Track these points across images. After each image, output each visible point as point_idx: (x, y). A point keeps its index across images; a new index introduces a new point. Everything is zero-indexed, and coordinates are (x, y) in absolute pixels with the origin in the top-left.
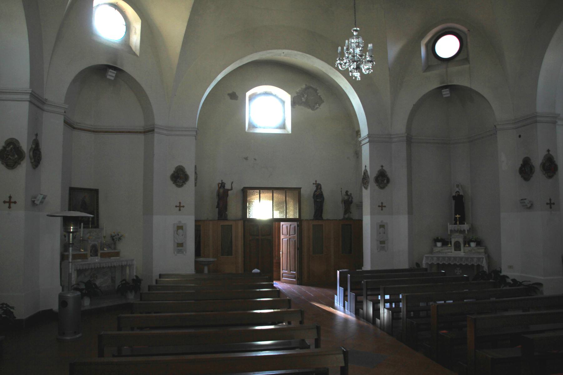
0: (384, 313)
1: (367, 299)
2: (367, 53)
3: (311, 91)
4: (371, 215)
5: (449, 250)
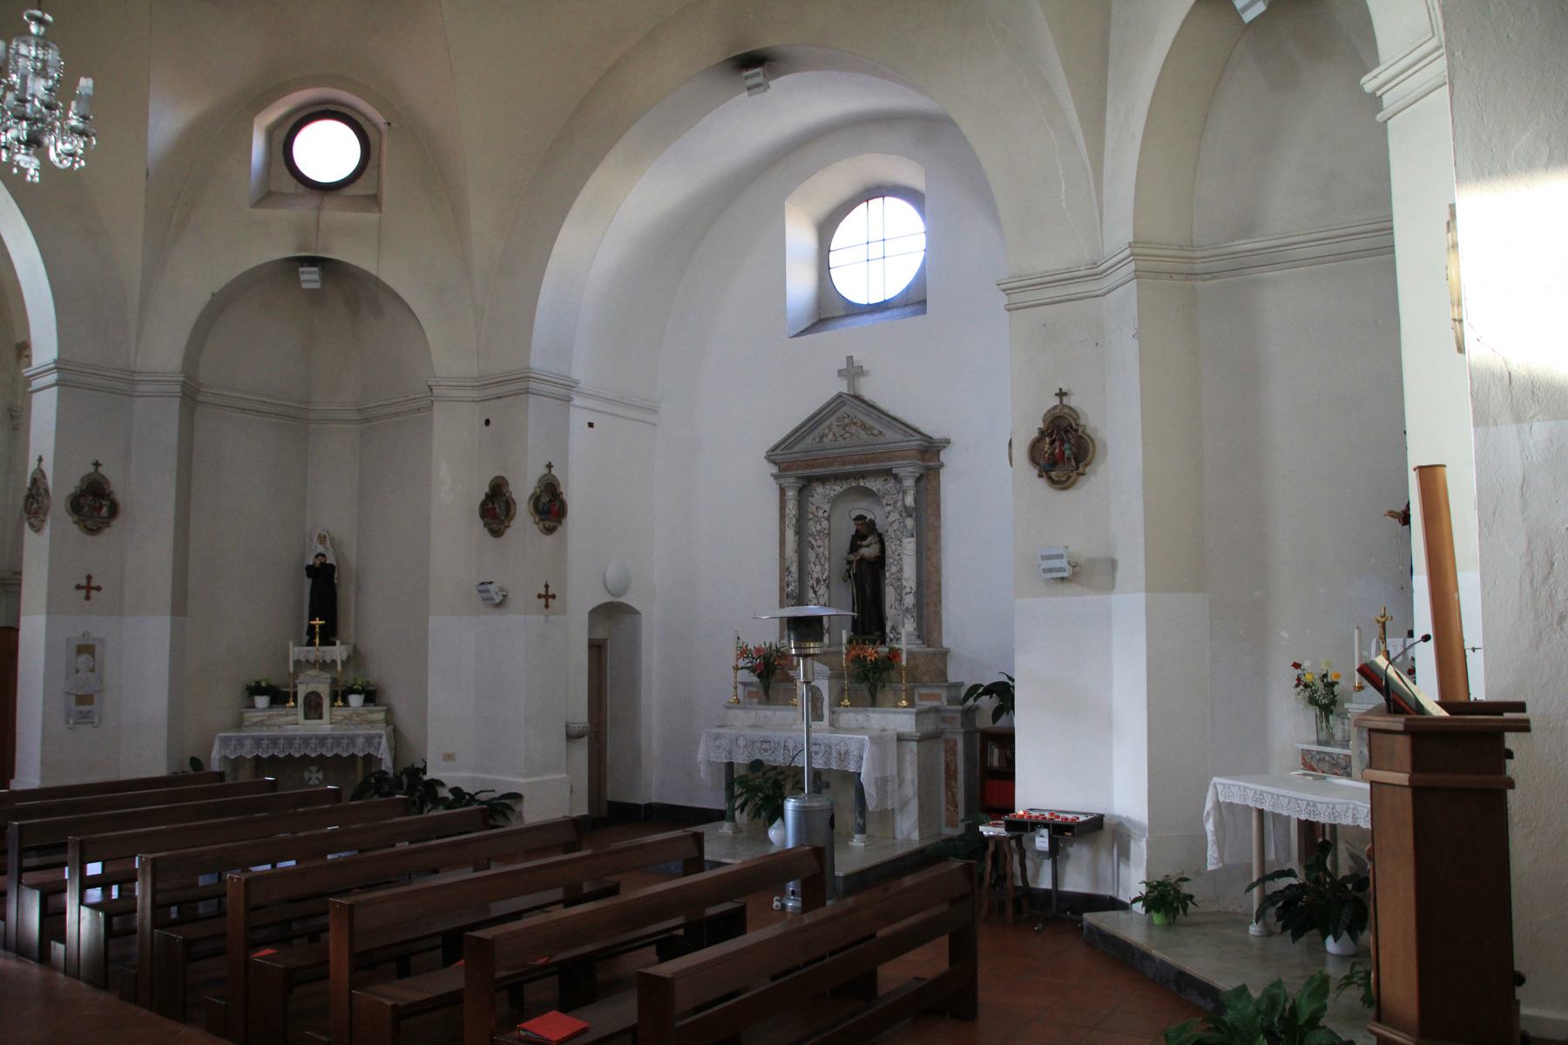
0: (82, 922)
1: (20, 882)
2: (73, 104)
4: (48, 613)
5: (290, 718)
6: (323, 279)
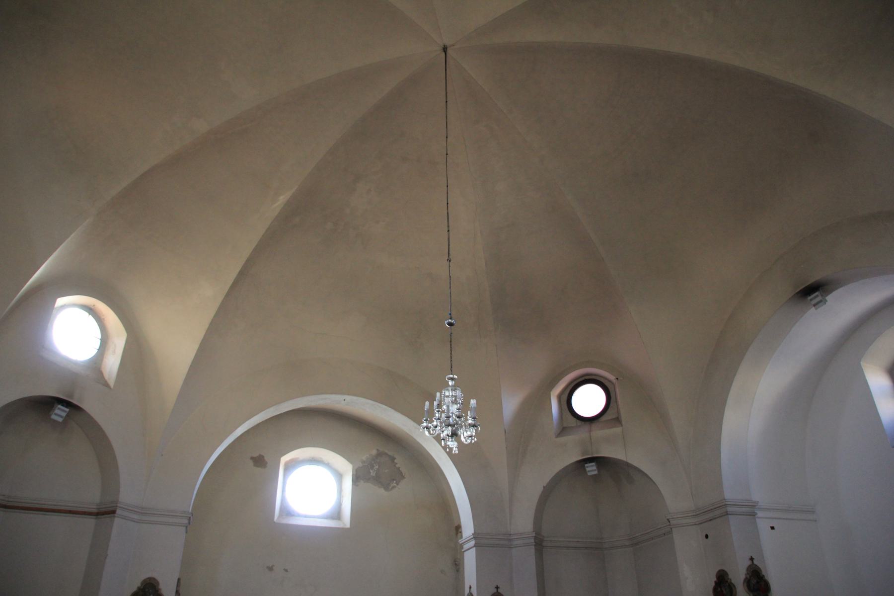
3: (385, 459)
6: (599, 468)
